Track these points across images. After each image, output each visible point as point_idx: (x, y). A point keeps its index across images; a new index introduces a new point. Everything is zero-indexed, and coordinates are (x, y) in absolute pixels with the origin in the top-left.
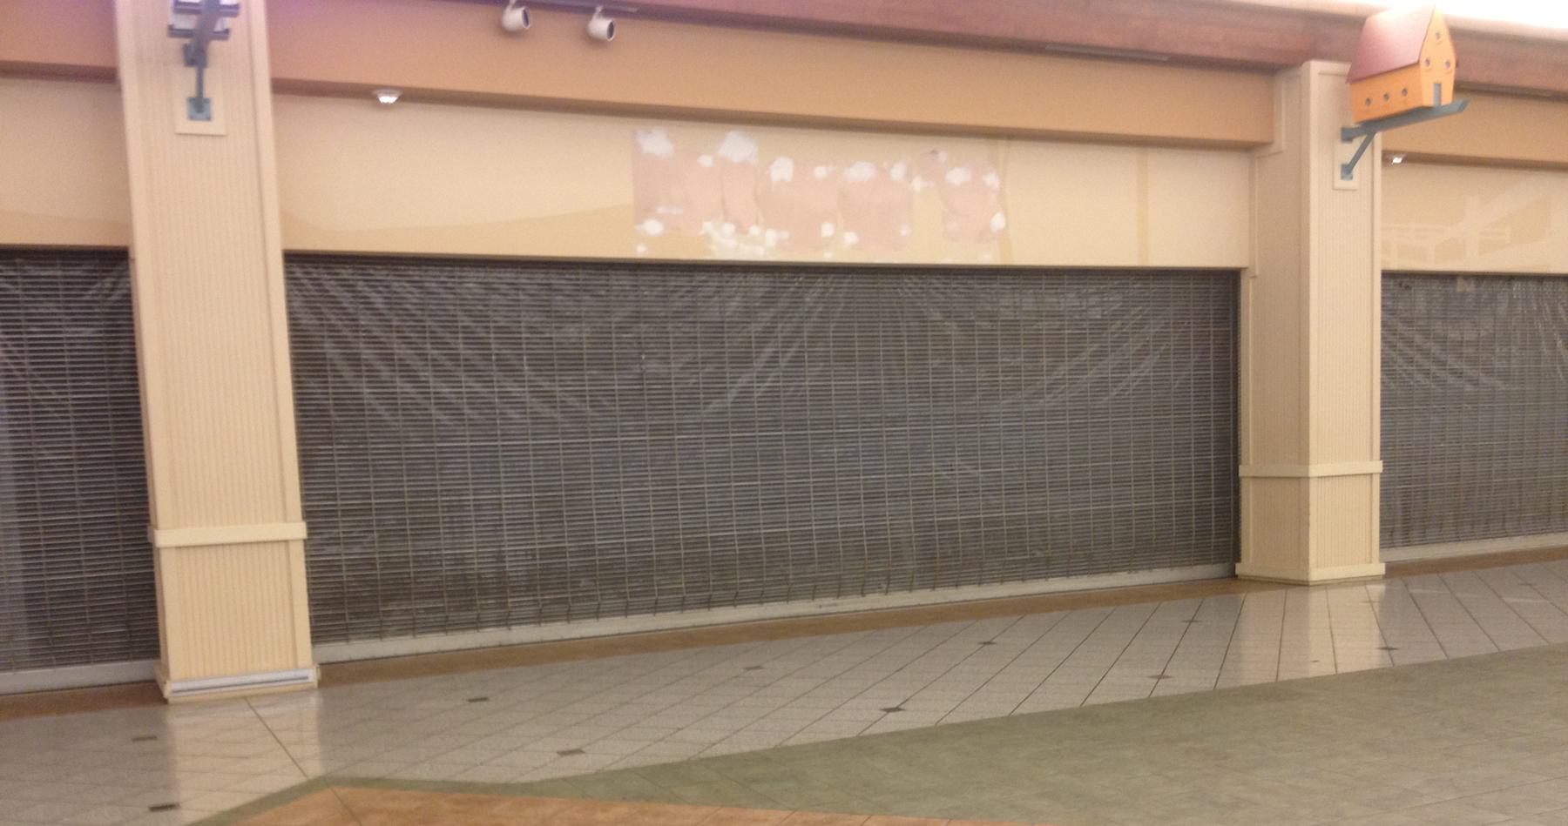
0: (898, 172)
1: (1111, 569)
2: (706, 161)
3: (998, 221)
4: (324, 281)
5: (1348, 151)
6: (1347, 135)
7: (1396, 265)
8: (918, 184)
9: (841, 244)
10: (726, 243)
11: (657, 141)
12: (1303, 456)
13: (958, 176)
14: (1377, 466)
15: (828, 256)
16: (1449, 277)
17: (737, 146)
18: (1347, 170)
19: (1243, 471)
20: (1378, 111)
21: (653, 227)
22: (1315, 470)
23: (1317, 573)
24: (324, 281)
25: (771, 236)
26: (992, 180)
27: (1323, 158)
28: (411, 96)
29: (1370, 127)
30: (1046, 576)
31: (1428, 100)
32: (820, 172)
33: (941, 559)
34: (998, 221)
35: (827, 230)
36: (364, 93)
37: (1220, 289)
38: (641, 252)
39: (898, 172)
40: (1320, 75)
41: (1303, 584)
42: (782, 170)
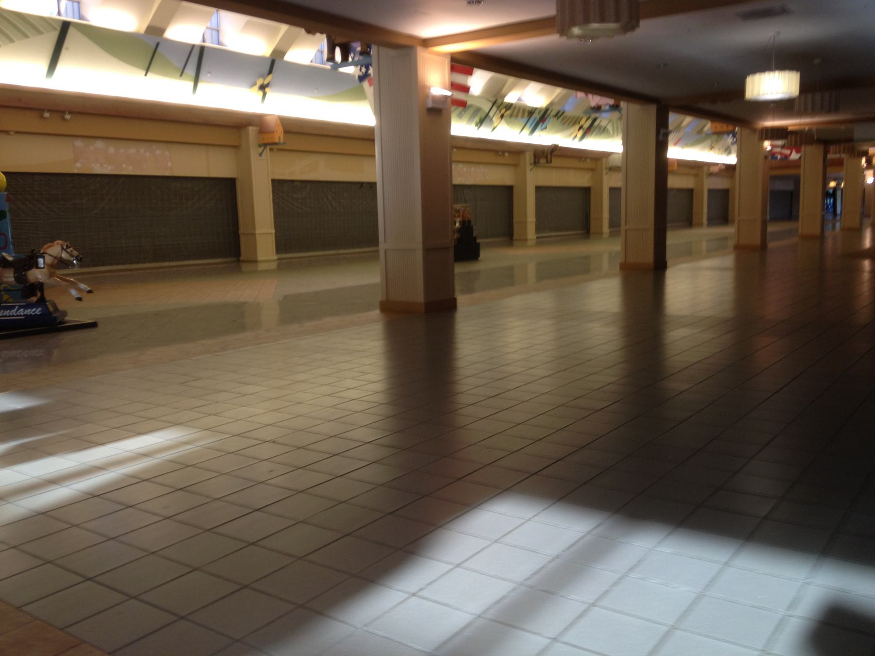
0: (142, 151)
1: (205, 258)
2: (92, 148)
3: (169, 164)
4: (278, 185)
5: (261, 150)
6: (260, 146)
7: (277, 177)
8: (148, 154)
9: (128, 169)
10: (98, 169)
11: (79, 143)
12: (254, 228)
13: (158, 152)
14: (273, 231)
15: (125, 173)
16: (293, 181)
17: (100, 144)
18: (261, 155)
19: (240, 232)
20: (266, 141)
21: (78, 165)
22: (258, 232)
23: (260, 258)
24: (278, 185)
25: (110, 168)
26: (167, 153)
27: (254, 152)
28: (17, 132)
29: (265, 145)
30: (189, 260)
31: (277, 141)
32: (122, 151)
33: (158, 256)
34: (169, 164)
35: (124, 166)
36: (7, 132)
37: (510, 189)
38: (76, 171)
39: (142, 151)
40: (252, 130)
41: (256, 262)
42: (112, 150)
